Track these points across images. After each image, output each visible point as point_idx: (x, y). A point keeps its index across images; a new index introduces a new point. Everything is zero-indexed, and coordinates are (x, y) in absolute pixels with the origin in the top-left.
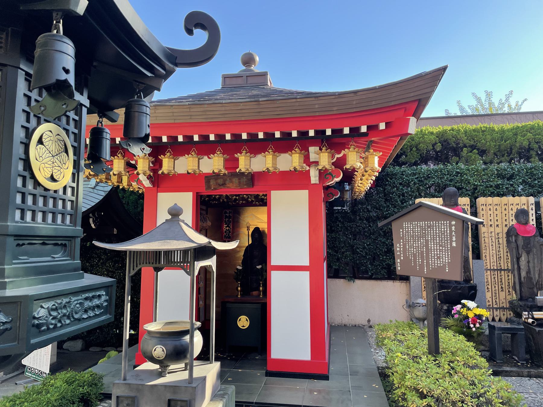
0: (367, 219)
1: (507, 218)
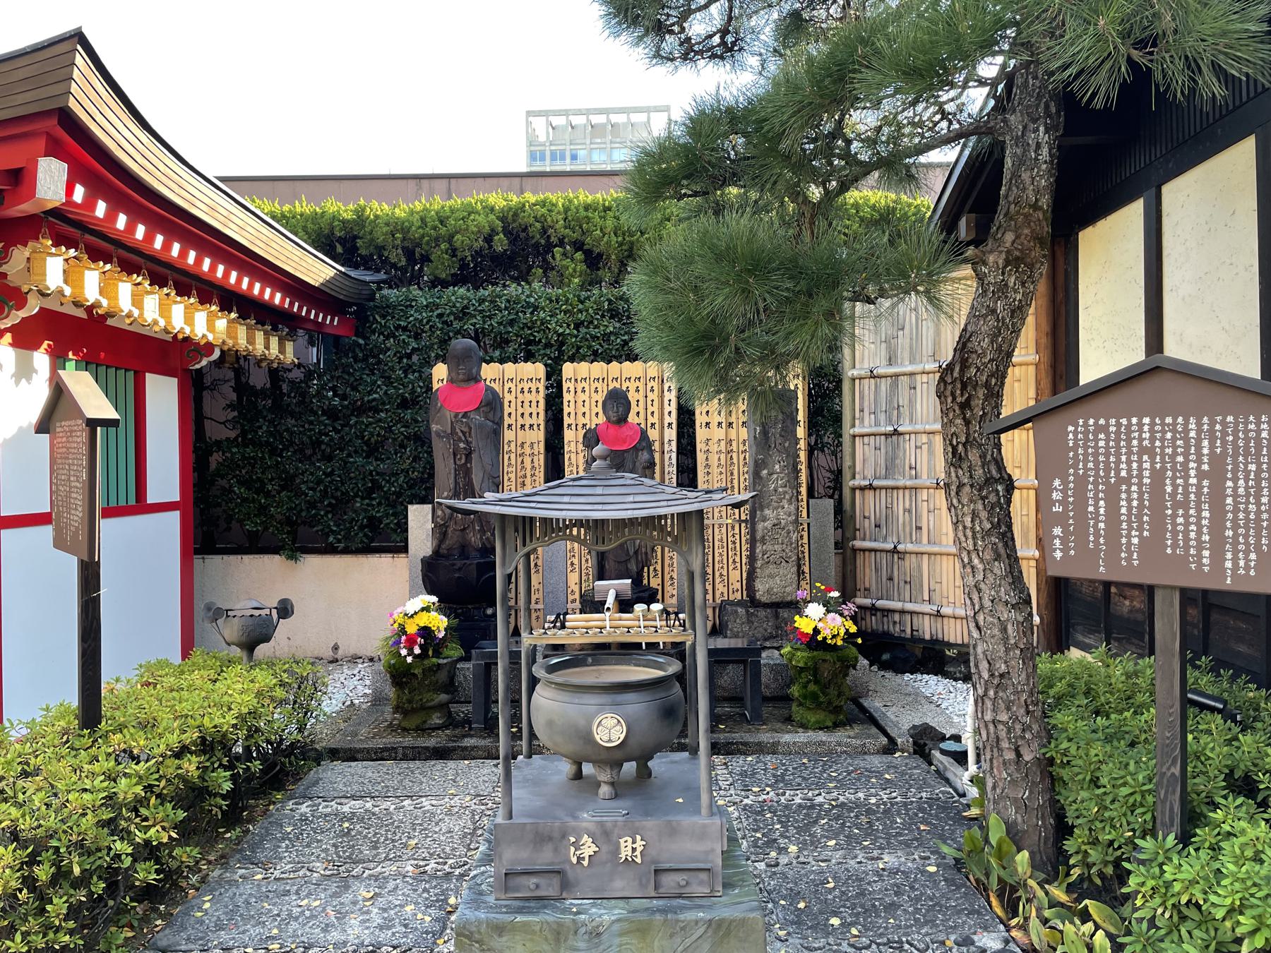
1: (586, 409)
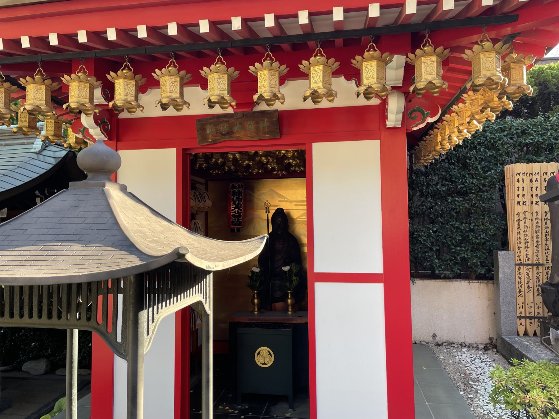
0: (433, 196)
